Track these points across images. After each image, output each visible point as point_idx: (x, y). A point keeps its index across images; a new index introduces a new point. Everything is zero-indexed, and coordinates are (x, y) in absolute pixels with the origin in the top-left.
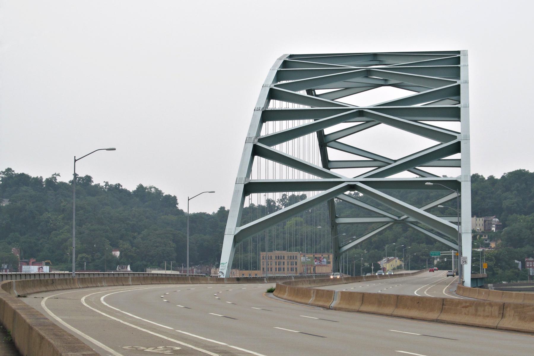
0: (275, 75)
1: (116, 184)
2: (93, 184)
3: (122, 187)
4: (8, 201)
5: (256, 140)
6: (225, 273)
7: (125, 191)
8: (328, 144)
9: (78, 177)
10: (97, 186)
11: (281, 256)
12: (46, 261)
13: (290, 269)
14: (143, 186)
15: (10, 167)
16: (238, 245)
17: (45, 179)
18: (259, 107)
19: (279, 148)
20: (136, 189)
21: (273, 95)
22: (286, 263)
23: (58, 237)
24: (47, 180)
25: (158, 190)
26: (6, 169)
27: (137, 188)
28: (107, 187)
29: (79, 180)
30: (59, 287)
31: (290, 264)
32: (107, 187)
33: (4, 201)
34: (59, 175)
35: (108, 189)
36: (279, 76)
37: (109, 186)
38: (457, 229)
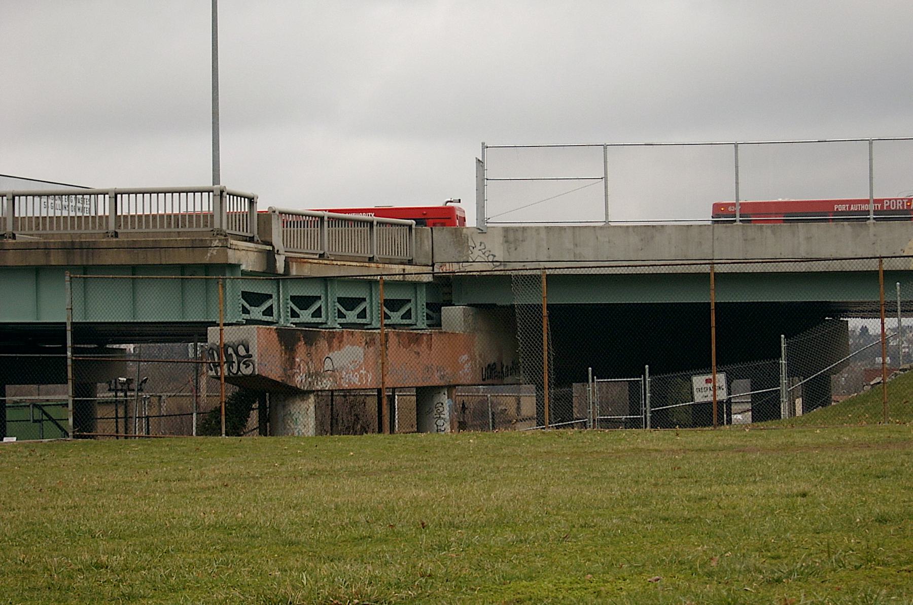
1: (339, 348)
7: (11, 384)
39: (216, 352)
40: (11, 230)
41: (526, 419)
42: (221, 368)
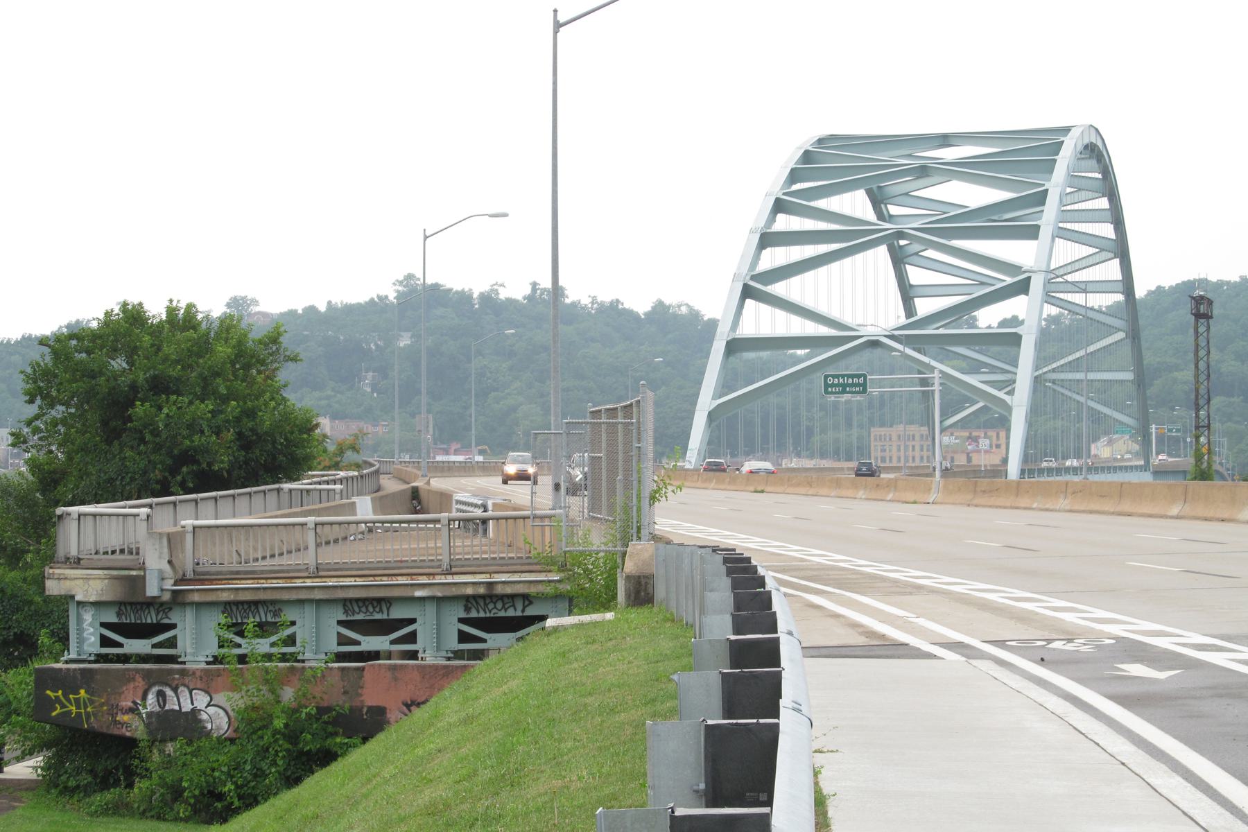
0: (785, 177)
1: (612, 300)
2: (568, 301)
3: (623, 305)
4: (410, 335)
5: (748, 278)
6: (693, 463)
7: (630, 314)
8: (905, 260)
9: (539, 289)
10: (574, 305)
11: (880, 436)
12: (480, 448)
13: (925, 458)
14: (663, 302)
15: (411, 272)
16: (714, 424)
17: (478, 294)
18: (757, 226)
19: (779, 289)
20: (650, 309)
21: (780, 206)
22: (917, 448)
23: (502, 403)
24: (482, 295)
25: (694, 310)
26: (405, 276)
27: (652, 307)
28: (595, 306)
29: (542, 294)
30: (456, 474)
31: (925, 450)
32: (595, 306)
33: (403, 337)
34: (502, 285)
35: (597, 309)
36: (794, 176)
37: (599, 304)
38: (1010, 404)
39: (1043, 646)
40: (76, 554)
41: (208, 684)
42: (1141, 466)
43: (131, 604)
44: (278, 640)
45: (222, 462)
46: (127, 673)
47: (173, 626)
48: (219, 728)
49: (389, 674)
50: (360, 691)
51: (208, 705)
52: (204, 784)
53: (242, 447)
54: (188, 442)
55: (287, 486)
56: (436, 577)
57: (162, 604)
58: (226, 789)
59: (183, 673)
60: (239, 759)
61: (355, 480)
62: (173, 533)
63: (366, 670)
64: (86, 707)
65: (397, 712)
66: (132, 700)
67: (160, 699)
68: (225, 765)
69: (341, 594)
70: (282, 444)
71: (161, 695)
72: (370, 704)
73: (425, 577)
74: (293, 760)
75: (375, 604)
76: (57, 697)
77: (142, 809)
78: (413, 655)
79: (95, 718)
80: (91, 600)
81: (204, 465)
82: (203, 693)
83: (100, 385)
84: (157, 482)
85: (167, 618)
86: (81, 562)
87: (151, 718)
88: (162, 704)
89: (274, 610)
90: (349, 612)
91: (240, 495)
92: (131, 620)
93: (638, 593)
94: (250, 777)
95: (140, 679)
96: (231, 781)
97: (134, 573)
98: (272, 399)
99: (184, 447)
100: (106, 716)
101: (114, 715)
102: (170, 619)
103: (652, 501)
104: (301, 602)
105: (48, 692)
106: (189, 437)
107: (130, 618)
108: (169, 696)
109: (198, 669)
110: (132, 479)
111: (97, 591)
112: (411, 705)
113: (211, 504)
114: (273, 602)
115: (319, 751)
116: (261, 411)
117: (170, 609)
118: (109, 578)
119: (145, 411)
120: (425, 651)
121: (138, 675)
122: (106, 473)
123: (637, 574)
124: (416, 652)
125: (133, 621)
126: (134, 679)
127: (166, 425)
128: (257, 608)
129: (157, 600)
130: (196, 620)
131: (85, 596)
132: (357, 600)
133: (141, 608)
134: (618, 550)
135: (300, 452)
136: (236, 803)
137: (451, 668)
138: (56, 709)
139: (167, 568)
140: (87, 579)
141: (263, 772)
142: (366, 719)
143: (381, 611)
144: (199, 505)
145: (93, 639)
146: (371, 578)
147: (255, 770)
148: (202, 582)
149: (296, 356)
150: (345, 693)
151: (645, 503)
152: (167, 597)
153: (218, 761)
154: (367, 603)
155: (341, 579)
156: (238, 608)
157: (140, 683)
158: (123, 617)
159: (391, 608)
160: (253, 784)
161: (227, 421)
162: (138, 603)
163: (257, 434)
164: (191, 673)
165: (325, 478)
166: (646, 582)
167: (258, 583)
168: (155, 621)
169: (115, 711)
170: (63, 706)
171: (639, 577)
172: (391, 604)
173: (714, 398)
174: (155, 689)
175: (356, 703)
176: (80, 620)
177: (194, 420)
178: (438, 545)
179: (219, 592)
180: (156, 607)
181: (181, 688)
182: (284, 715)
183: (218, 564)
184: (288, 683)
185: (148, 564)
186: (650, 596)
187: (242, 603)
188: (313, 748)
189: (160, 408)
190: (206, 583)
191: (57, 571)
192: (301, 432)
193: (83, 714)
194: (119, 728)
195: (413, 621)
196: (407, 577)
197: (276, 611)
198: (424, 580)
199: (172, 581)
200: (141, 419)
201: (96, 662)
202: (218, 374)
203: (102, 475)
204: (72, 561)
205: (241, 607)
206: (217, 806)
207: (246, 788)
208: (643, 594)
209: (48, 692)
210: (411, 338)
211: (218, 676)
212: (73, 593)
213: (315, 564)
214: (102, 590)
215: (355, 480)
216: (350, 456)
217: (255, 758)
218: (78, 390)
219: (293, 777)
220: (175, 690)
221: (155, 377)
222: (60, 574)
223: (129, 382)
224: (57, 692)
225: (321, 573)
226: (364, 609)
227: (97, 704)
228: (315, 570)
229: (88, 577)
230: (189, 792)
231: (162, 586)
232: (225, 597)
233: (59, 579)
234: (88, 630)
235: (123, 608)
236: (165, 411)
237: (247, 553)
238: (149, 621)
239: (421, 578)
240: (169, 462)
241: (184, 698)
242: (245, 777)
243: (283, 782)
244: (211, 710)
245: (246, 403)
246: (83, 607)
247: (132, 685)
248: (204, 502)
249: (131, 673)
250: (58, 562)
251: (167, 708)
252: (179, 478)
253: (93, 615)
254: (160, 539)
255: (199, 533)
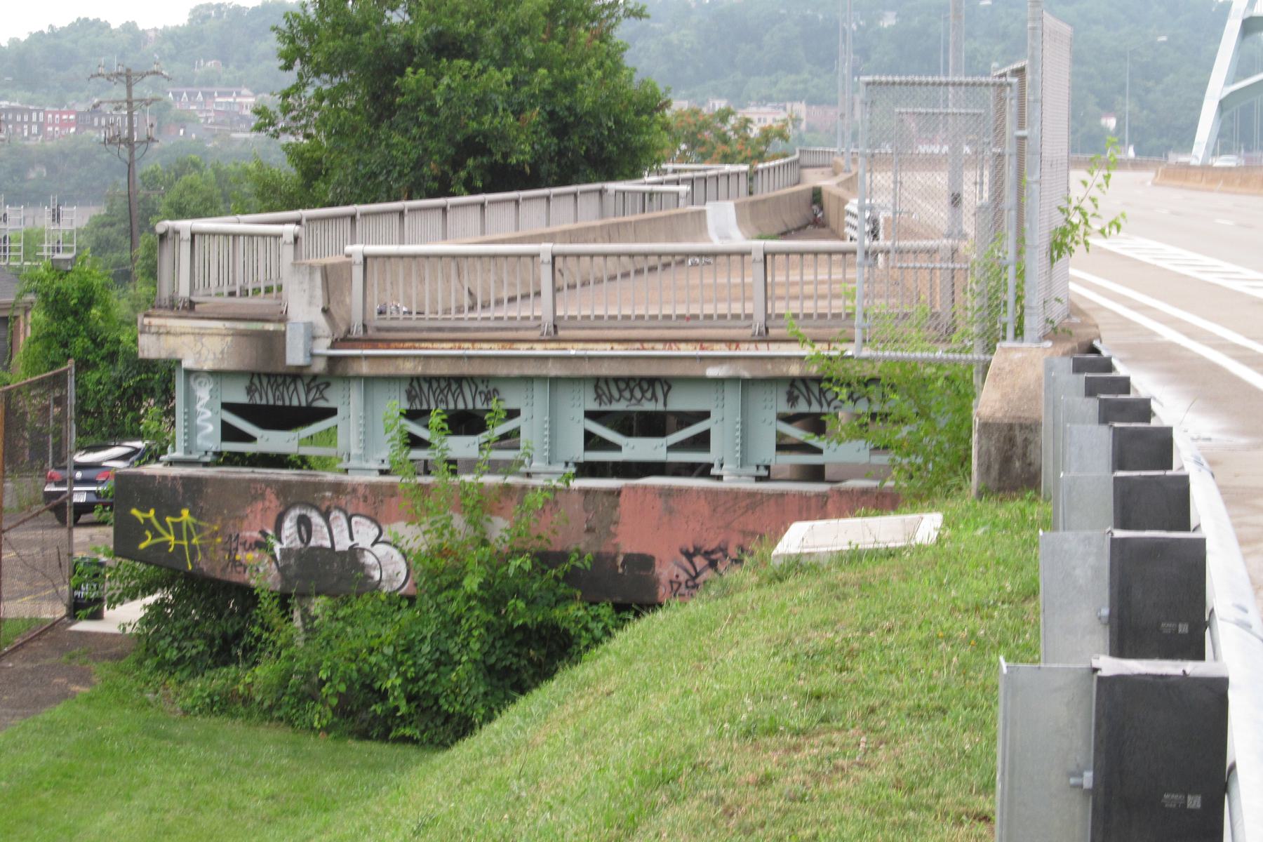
16: (1226, 114)
43: (268, 375)
44: (485, 443)
45: (523, 152)
46: (252, 485)
47: (332, 412)
48: (391, 580)
49: (659, 503)
50: (612, 528)
51: (376, 542)
52: (355, 675)
53: (554, 132)
54: (474, 125)
55: (612, 186)
56: (742, 346)
57: (315, 377)
58: (389, 684)
59: (338, 488)
60: (413, 635)
61: (772, 171)
62: (333, 266)
63: (623, 494)
64: (190, 537)
65: (672, 565)
66: (259, 529)
67: (303, 528)
68: (389, 645)
69: (589, 370)
70: (609, 129)
71: (303, 522)
72: (629, 551)
73: (723, 346)
74: (501, 638)
75: (645, 386)
76: (147, 520)
77: (266, 704)
78: (704, 470)
79: (205, 555)
80: (206, 368)
81: (498, 157)
82: (368, 522)
83: (362, 44)
84: (435, 178)
85: (323, 398)
86: (196, 306)
87: (289, 559)
88: (305, 537)
89: (486, 390)
90: (604, 398)
91: (584, 192)
92: (267, 400)
93: (1006, 460)
94: (428, 666)
95: (273, 497)
96: (398, 670)
97: (270, 327)
98: (601, 65)
99: (470, 131)
100: (221, 553)
101: (232, 552)
102: (327, 400)
103: (1055, 253)
104: (529, 380)
105: (135, 512)
106: (477, 118)
107: (267, 398)
108: (317, 525)
109: (360, 484)
110: (401, 174)
111: (214, 354)
112: (694, 555)
113: (475, 214)
114: (486, 379)
115: (541, 626)
116: (583, 83)
117: (328, 385)
118: (233, 335)
119: (418, 81)
120: (722, 465)
121: (268, 490)
122: (366, 165)
123: (1006, 421)
124: (711, 466)
125: (271, 402)
126: (263, 496)
127: (447, 101)
128: (460, 386)
129: (305, 371)
130: (365, 409)
131: (197, 361)
132: (617, 380)
133: (284, 382)
134: (973, 360)
135: (638, 140)
136: (403, 709)
137: (759, 497)
138: (146, 538)
139: (320, 320)
140: (200, 334)
141: (451, 657)
142: (622, 575)
143: (654, 397)
144: (406, 219)
145: (210, 428)
146: (638, 345)
147: (438, 654)
148: (373, 343)
149: (642, 10)
150: (590, 530)
151: (1036, 261)
152: (319, 366)
153: (379, 636)
154: (632, 384)
155: (590, 346)
156: (430, 386)
157: (273, 503)
158: (257, 395)
159: (670, 394)
160: (431, 677)
161: (533, 96)
162: (281, 375)
163: (576, 115)
164: (349, 489)
165: (689, 175)
166: (1026, 439)
167: (459, 348)
168: (304, 404)
169: (234, 545)
170: (156, 534)
171: (1011, 427)
172: (670, 388)
173: (1227, 84)
174: (295, 513)
175: (606, 548)
176: (190, 399)
177: (485, 93)
178: (805, 278)
179: (400, 362)
180: (306, 381)
181: (335, 514)
182: (482, 569)
183: (414, 313)
184: (499, 511)
185: (290, 314)
186: (1032, 469)
187: (438, 379)
188: (529, 622)
189: (439, 76)
190: (380, 345)
191: (155, 321)
192: (638, 113)
193: (186, 548)
194: (240, 573)
195: (705, 415)
196: (694, 345)
197: (489, 392)
198: (721, 350)
199: (328, 342)
200: (412, 91)
201: (217, 464)
202: (523, 31)
203: (361, 167)
204: (181, 305)
205: (435, 385)
206: (375, 710)
207: (421, 683)
208: (1017, 464)
209: (135, 512)
210: (897, 16)
211: (392, 496)
212: (179, 356)
213: (551, 319)
214: (222, 352)
215: (772, 171)
216: (778, 144)
217: (439, 634)
218: (336, 50)
219: (499, 666)
220: (326, 515)
221: (439, 35)
222: (159, 327)
223: (402, 40)
224: (148, 512)
225: (561, 333)
226: (627, 394)
227: (207, 533)
228: (552, 329)
229: (202, 331)
230: (330, 687)
231: (312, 349)
232: (408, 368)
233: (158, 334)
234: (203, 413)
235: (256, 381)
236: (446, 80)
237: (486, 292)
238: (295, 403)
239: (716, 346)
240: (450, 151)
241: (339, 529)
242: (422, 665)
243: (480, 675)
244: (381, 549)
245: (562, 72)
246: (196, 378)
247: (259, 505)
248: (528, 203)
249: (259, 486)
250: (160, 307)
251: (313, 543)
252: (463, 174)
253: (211, 390)
254: (310, 274)
255: (374, 267)
